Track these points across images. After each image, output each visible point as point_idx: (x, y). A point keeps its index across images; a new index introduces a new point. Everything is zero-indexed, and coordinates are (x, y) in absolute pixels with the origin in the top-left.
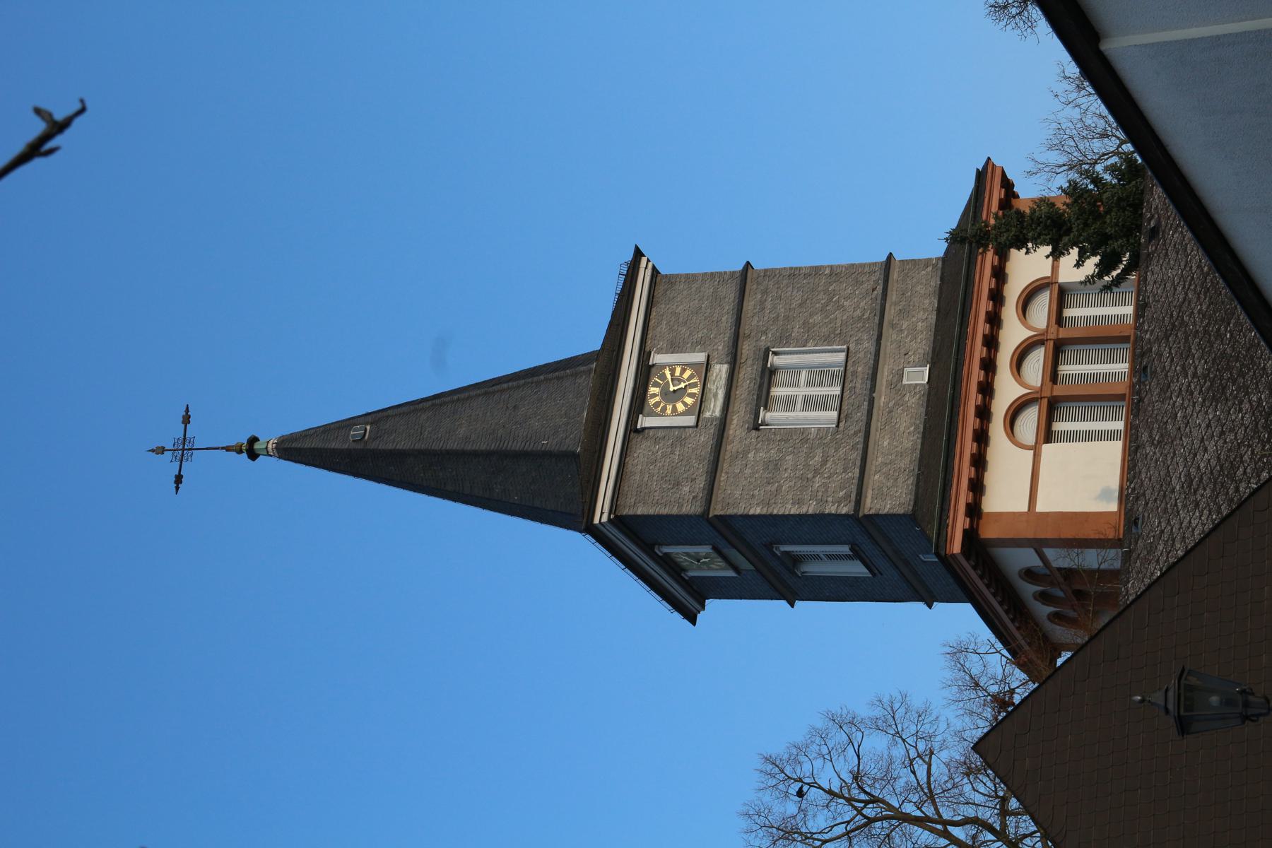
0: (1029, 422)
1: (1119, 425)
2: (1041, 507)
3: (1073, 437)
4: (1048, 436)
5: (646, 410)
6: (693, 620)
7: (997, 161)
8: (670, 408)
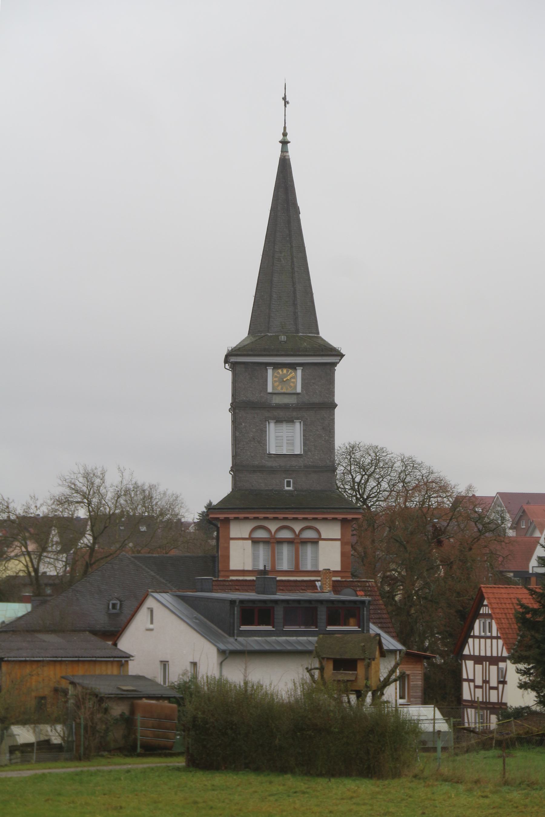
0: (261, 534)
4: (255, 542)
8: (276, 379)
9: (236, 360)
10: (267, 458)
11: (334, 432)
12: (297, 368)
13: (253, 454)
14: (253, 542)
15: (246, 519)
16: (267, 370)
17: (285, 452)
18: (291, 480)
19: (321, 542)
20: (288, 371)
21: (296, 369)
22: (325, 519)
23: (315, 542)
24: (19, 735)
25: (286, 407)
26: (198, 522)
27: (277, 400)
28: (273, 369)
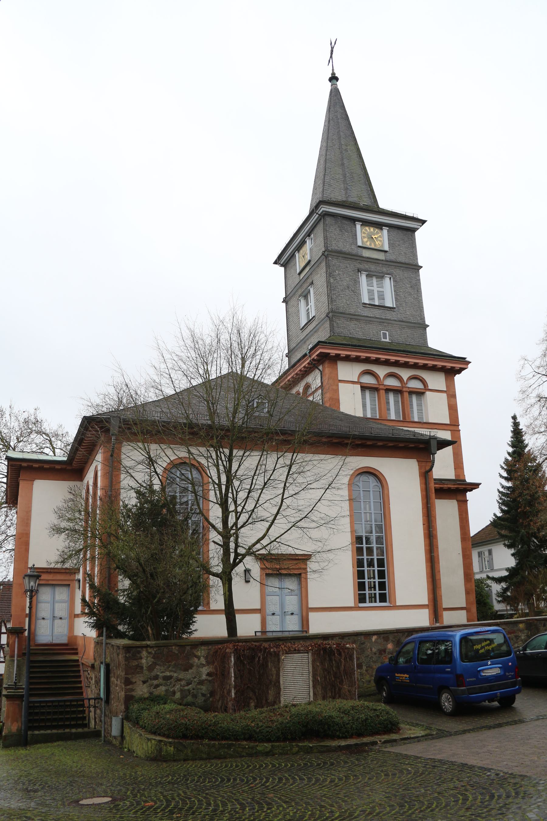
0: (368, 380)
1: (369, 415)
2: (341, 385)
3: (364, 398)
4: (364, 388)
5: (363, 227)
6: (275, 263)
7: (470, 365)
8: (365, 235)
9: (327, 210)
10: (362, 307)
11: (421, 291)
13: (348, 303)
14: (362, 387)
16: (355, 225)
18: (387, 333)
19: (428, 393)
20: (374, 230)
21: (382, 229)
23: (420, 394)
25: (375, 261)
26: (196, 614)
28: (361, 225)
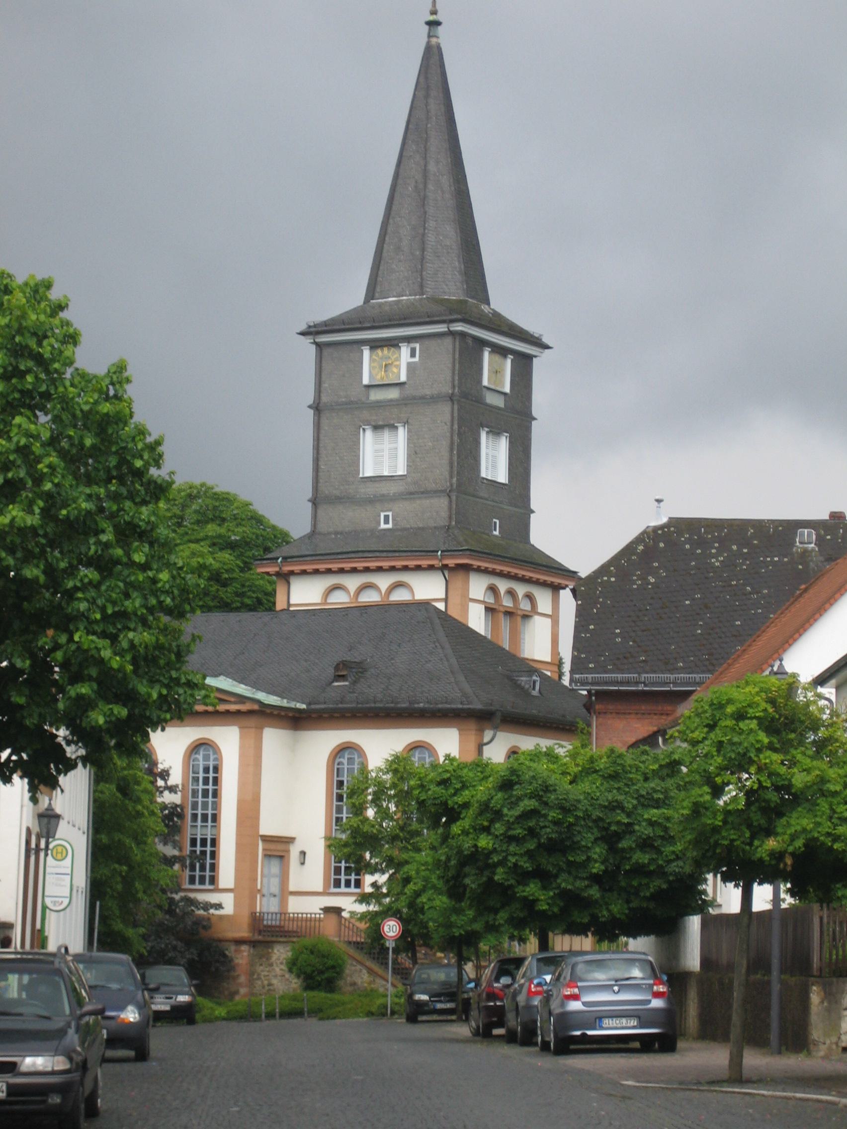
12: (400, 345)
15: (316, 572)
17: (386, 473)
22: (418, 568)
24: (62, 791)
27: (376, 396)
